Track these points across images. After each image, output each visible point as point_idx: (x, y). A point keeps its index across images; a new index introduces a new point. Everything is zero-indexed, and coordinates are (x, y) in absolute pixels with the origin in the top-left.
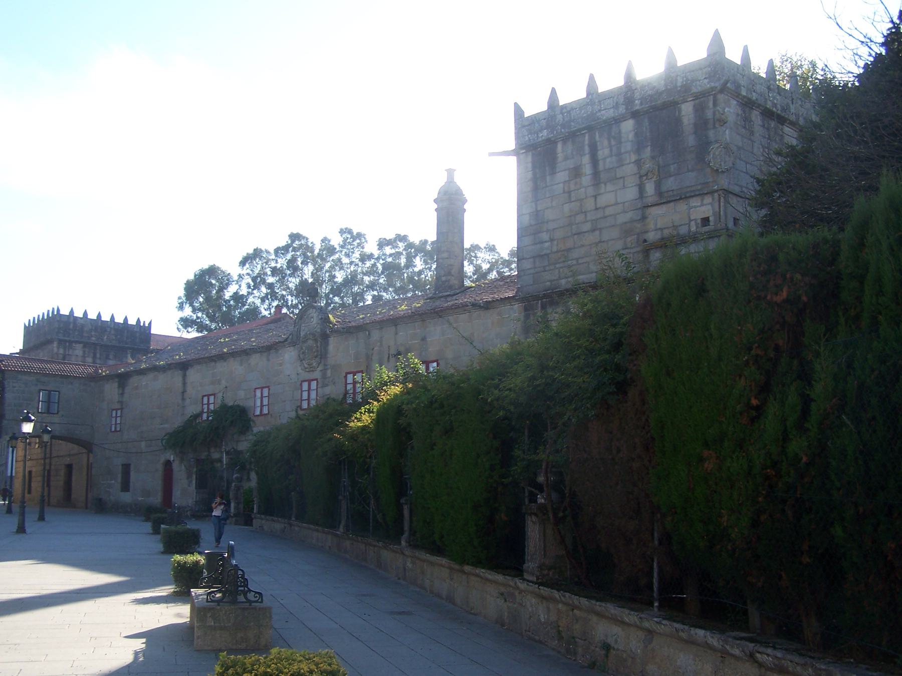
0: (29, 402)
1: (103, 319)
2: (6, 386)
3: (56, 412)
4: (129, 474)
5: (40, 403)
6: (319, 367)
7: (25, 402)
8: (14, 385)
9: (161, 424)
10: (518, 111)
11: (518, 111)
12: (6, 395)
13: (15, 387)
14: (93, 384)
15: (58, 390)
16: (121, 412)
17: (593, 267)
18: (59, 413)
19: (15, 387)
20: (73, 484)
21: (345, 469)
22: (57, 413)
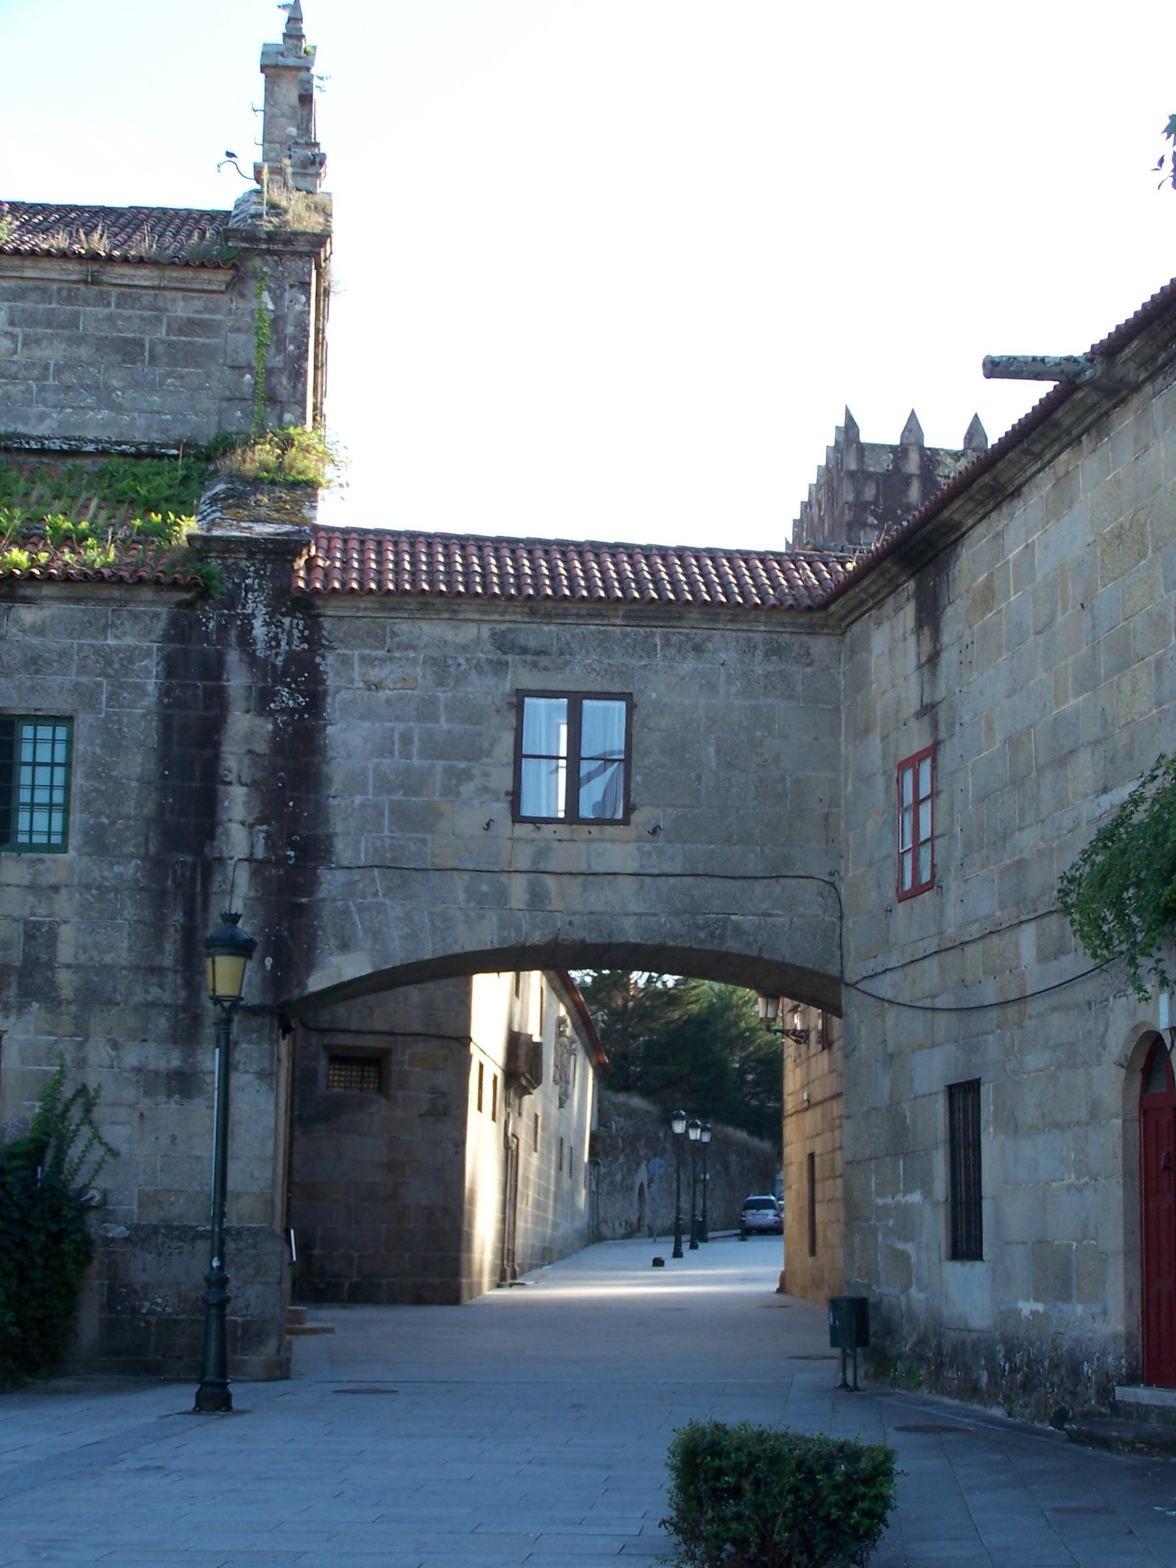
0: (463, 765)
1: (865, 438)
2: (331, 682)
3: (619, 815)
4: (975, 1145)
5: (563, 752)
6: (238, 1056)
7: (440, 765)
8: (375, 674)
9: (1105, 790)
10: (850, 429)
11: (850, 429)
12: (330, 730)
13: (378, 686)
14: (819, 646)
15: (617, 688)
16: (934, 768)
17: (638, 799)
18: (635, 817)
19: (378, 686)
20: (988, 1186)
21: (967, 1185)
22: (626, 821)
